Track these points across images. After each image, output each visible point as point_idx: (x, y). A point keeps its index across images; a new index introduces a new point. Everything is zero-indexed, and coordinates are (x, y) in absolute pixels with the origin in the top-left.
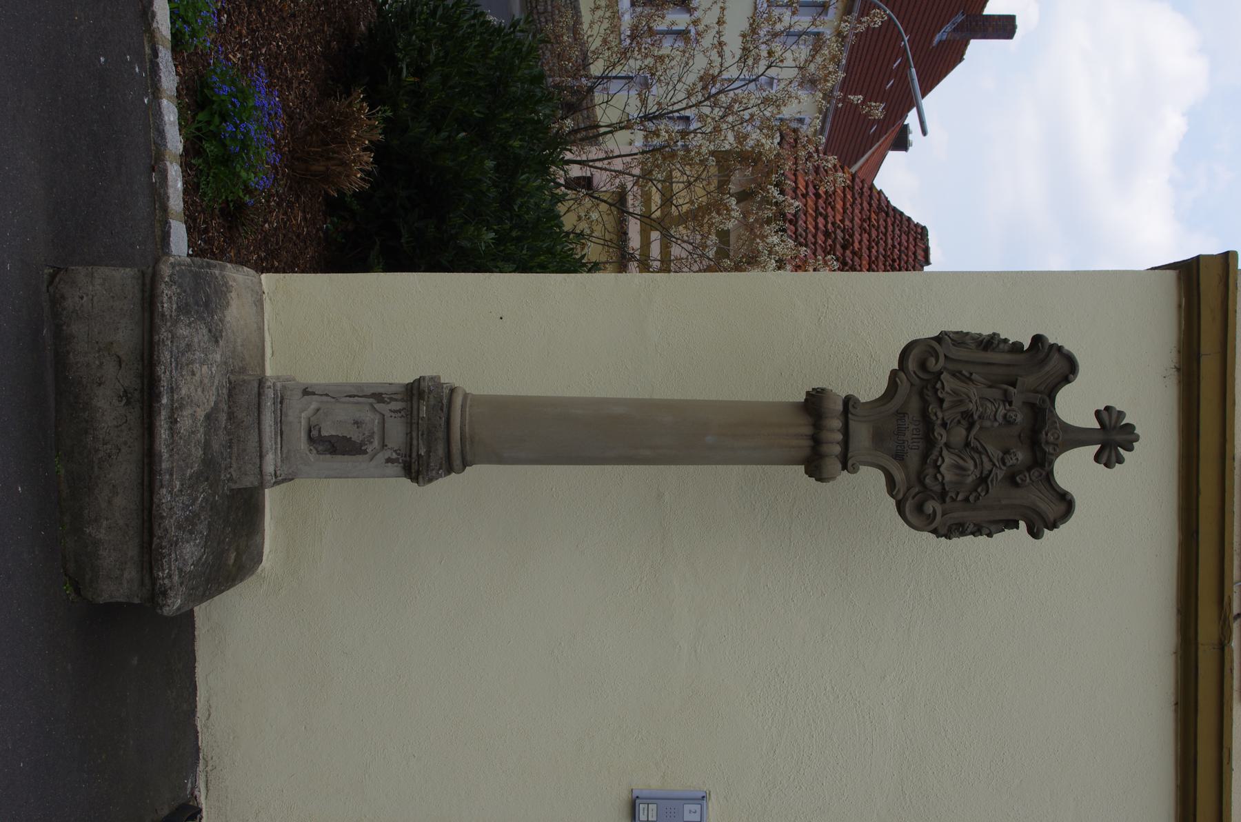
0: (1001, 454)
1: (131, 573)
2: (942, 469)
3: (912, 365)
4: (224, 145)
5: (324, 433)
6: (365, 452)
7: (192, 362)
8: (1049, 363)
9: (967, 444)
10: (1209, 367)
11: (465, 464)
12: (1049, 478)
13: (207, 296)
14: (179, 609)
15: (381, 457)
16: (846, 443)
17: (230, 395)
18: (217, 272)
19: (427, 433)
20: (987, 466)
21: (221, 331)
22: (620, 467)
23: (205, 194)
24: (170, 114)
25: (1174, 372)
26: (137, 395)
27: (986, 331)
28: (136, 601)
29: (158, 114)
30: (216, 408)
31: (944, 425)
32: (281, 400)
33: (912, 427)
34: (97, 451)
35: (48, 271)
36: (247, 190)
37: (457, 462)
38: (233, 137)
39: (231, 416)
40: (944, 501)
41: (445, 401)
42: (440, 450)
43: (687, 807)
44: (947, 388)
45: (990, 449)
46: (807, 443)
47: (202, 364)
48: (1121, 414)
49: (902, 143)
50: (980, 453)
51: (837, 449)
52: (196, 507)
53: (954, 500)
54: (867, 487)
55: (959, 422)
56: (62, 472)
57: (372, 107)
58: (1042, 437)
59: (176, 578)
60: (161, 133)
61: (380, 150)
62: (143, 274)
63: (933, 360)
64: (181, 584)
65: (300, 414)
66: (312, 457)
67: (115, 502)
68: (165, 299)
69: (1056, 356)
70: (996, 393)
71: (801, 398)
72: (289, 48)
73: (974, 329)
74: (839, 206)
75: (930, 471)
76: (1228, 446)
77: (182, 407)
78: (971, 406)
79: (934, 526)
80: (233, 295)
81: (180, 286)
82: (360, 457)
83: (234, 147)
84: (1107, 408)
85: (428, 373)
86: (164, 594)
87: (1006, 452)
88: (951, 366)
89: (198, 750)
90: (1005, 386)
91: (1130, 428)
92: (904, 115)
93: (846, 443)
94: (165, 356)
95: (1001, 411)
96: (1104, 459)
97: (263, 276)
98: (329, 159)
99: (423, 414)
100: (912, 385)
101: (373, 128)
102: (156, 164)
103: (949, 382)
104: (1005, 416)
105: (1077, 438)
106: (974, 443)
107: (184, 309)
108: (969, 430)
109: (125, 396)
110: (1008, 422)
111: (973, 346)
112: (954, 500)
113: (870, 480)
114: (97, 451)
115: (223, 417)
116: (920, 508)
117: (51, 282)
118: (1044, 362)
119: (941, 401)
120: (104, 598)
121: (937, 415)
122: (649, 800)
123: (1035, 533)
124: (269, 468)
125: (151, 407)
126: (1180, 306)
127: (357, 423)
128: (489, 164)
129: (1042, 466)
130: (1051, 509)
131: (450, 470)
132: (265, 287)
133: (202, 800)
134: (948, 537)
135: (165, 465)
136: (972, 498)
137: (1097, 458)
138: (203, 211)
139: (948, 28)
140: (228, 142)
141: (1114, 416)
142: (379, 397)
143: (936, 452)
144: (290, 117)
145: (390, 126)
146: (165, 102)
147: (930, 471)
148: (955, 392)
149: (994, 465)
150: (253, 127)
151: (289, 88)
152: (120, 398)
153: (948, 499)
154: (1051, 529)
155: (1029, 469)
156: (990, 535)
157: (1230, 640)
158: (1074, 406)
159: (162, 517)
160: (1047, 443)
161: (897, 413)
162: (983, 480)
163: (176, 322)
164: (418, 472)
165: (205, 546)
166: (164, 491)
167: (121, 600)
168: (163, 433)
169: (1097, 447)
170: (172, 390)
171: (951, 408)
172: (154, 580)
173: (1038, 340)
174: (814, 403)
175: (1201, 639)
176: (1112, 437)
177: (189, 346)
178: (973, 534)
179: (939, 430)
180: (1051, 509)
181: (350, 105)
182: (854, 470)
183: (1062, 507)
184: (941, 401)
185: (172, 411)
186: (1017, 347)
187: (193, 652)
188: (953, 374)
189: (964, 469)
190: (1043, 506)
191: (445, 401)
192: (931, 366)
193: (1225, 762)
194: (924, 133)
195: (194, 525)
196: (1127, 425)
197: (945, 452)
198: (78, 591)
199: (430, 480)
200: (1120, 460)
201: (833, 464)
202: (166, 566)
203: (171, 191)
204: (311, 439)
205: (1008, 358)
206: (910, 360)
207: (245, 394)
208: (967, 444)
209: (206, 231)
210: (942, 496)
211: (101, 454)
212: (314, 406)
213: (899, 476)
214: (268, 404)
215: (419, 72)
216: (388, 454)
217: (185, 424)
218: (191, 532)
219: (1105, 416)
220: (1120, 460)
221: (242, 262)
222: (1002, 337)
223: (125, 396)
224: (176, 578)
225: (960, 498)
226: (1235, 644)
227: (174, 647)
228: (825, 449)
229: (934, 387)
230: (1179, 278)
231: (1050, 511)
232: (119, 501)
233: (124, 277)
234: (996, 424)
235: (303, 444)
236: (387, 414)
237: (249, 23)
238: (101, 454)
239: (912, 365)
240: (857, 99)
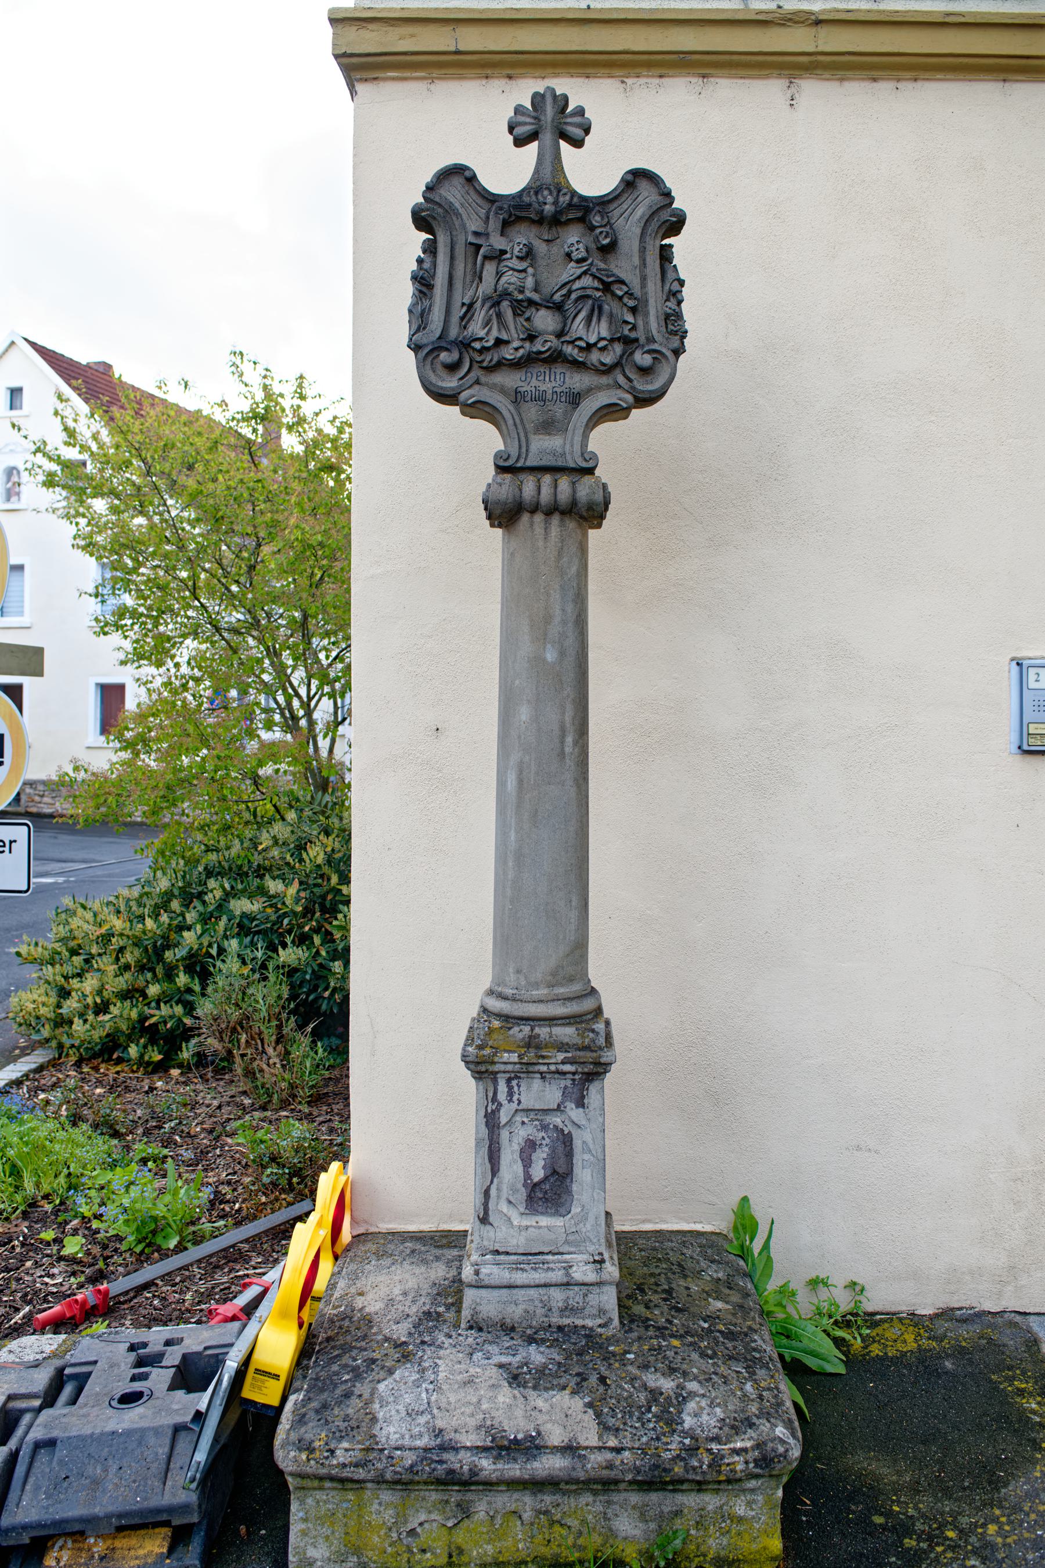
0: (572, 264)
2: (592, 341)
3: (450, 383)
10: (472, 40)
12: (604, 203)
19: (544, 1046)
33: (534, 383)
40: (636, 340)
44: (482, 333)
45: (565, 278)
48: (519, 110)
50: (570, 292)
51: (564, 484)
53: (634, 328)
54: (616, 448)
55: (528, 319)
58: (548, 209)
71: (499, 532)
75: (595, 357)
76: (570, 16)
84: (511, 129)
90: (480, 258)
100: (477, 382)
111: (427, 303)
113: (604, 440)
118: (450, 211)
119: (499, 342)
120: (776, 1545)
123: (676, 225)
136: (631, 303)
137: (578, 143)
142: (491, 1121)
143: (568, 350)
147: (595, 357)
149: (585, 273)
153: (633, 335)
156: (682, 283)
157: (811, 13)
158: (508, 171)
161: (515, 402)
169: (563, 145)
171: (507, 329)
173: (421, 220)
174: (503, 514)
176: (552, 126)
178: (679, 303)
179: (538, 346)
180: (646, 197)
182: (594, 456)
183: (644, 186)
184: (499, 342)
186: (430, 248)
192: (451, 360)
193: (963, 20)
200: (580, 111)
201: (585, 489)
206: (444, 385)
212: (504, 1207)
222: (414, 266)
225: (630, 318)
226: (816, 7)
234: (530, 270)
239: (450, 383)
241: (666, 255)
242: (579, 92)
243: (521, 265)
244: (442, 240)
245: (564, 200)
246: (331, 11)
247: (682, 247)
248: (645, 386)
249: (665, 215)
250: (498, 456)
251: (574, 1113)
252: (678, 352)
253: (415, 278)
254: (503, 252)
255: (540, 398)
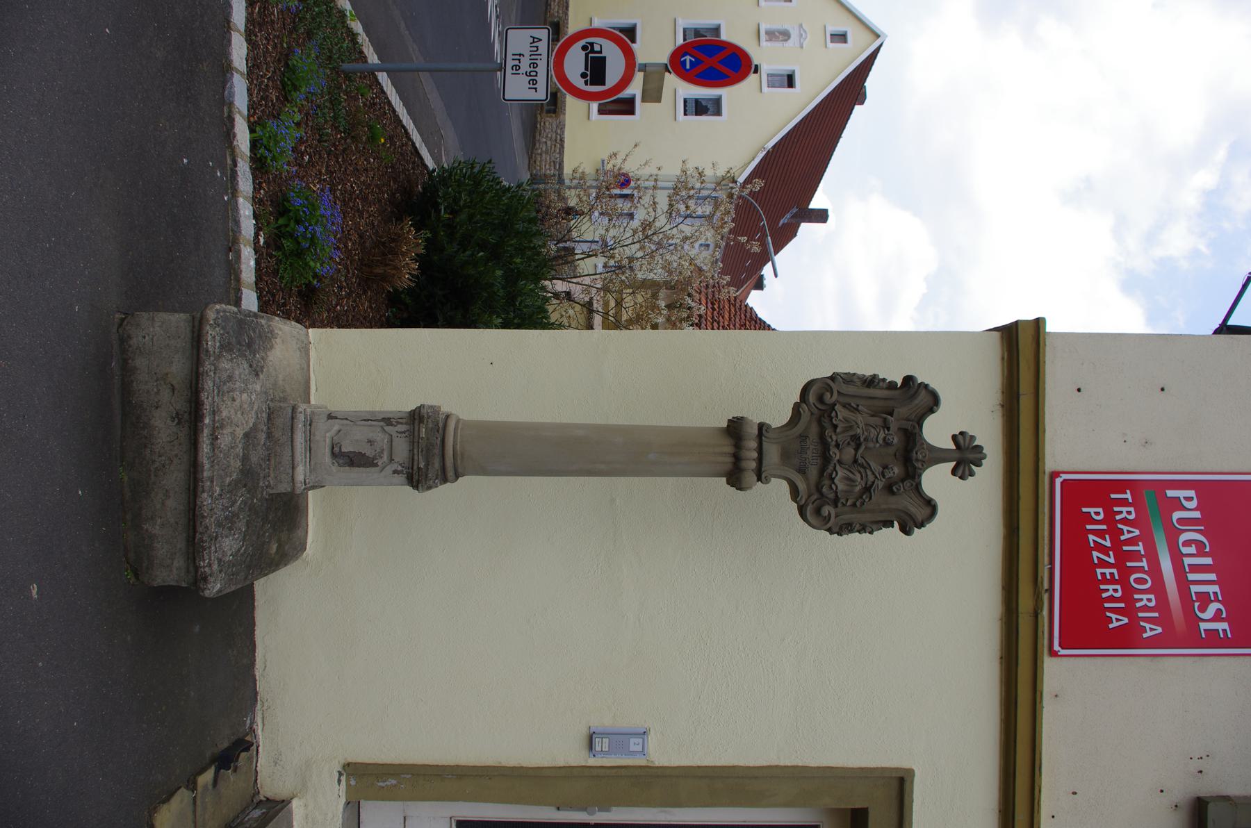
1: (179, 562)
3: (812, 398)
4: (299, 243)
5: (344, 450)
6: (376, 465)
7: (233, 390)
8: (916, 397)
9: (855, 461)
10: (1025, 403)
11: (457, 476)
12: (918, 488)
13: (251, 339)
14: (220, 591)
15: (389, 469)
16: (760, 460)
17: (269, 419)
18: (263, 322)
19: (427, 451)
20: (871, 478)
21: (262, 367)
22: (582, 478)
23: (282, 278)
24: (246, 210)
25: (999, 408)
26: (186, 416)
27: (868, 373)
28: (184, 585)
29: (236, 209)
30: (255, 428)
31: (837, 446)
32: (310, 423)
34: (154, 462)
35: (118, 316)
36: (315, 276)
37: (450, 474)
38: (304, 237)
39: (269, 435)
41: (441, 425)
42: (437, 465)
43: (632, 741)
45: (873, 465)
46: (730, 460)
47: (242, 392)
48: (973, 438)
49: (759, 285)
51: (754, 465)
52: (235, 509)
53: (844, 505)
54: (774, 496)
56: (126, 478)
57: (417, 230)
58: (912, 455)
59: (215, 567)
60: (237, 222)
61: (424, 261)
62: (193, 318)
63: (828, 395)
64: (221, 571)
65: (325, 434)
66: (335, 468)
67: (166, 506)
68: (209, 338)
69: (923, 392)
70: (877, 421)
71: (725, 425)
72: (361, 191)
73: (860, 372)
74: (727, 316)
75: (827, 482)
77: (222, 426)
78: (859, 431)
79: (829, 525)
80: (278, 340)
81: (223, 328)
82: (373, 469)
83: (305, 244)
84: (962, 433)
85: (429, 402)
86: (205, 579)
87: (885, 467)
88: (842, 400)
89: (256, 693)
91: (979, 449)
92: (761, 268)
93: (760, 460)
94: (209, 384)
95: (882, 435)
96: (960, 473)
97: (310, 330)
98: (386, 265)
99: (423, 434)
101: (418, 245)
102: (232, 245)
103: (841, 412)
104: (884, 439)
105: (938, 456)
106: (860, 460)
107: (226, 347)
108: (857, 449)
109: (177, 417)
110: (887, 443)
112: (844, 505)
113: (778, 489)
114: (154, 462)
115: (262, 437)
116: (818, 511)
117: (120, 325)
119: (835, 427)
120: (158, 582)
121: (832, 438)
122: (604, 734)
123: (906, 530)
124: (300, 477)
125: (196, 425)
126: (1003, 358)
127: (370, 442)
128: (499, 273)
129: (913, 478)
130: (919, 512)
131: (445, 480)
132: (311, 339)
133: (259, 732)
134: (840, 534)
135: (205, 474)
137: (954, 472)
138: (281, 289)
139: (788, 216)
140: (300, 239)
141: (968, 439)
142: (388, 421)
143: (831, 468)
144: (361, 236)
145: (431, 244)
146: (241, 200)
148: (846, 420)
150: (319, 229)
151: (361, 216)
152: (173, 419)
154: (919, 528)
155: (903, 481)
156: (871, 533)
159: (203, 517)
160: (917, 460)
162: (867, 489)
163: (219, 357)
164: (418, 482)
165: (244, 540)
166: (205, 495)
167: (172, 583)
168: (205, 448)
169: (953, 464)
170: (214, 413)
171: (843, 432)
172: (197, 568)
173: (908, 380)
174: (735, 428)
175: (1021, 609)
176: (965, 456)
177: (230, 378)
178: (859, 532)
179: (833, 450)
180: (919, 512)
181: (402, 229)
182: (767, 481)
183: (928, 511)
184: (835, 427)
185: (214, 429)
186: (892, 385)
187: (253, 618)
188: (844, 406)
189: (853, 481)
190: (913, 510)
191: (441, 425)
194: (776, 276)
195: (233, 523)
196: (977, 446)
197: (838, 467)
198: (136, 576)
199: (429, 488)
200: (972, 474)
201: (750, 477)
202: (206, 557)
203: (243, 267)
204: (333, 454)
205: (886, 393)
207: (281, 418)
208: (855, 461)
209: (284, 305)
210: (835, 503)
211: (157, 464)
212: (336, 428)
213: (802, 486)
214: (300, 426)
215: (454, 213)
216: (395, 466)
217: (225, 440)
218: (230, 529)
219: (960, 438)
220: (972, 474)
221: (287, 316)
223: (177, 417)
224: (215, 567)
227: (238, 611)
228: (744, 464)
229: (830, 416)
230: (1002, 337)
231: (916, 514)
232: (170, 503)
233: (178, 320)
235: (328, 458)
236: (394, 435)
237: (328, 166)
238: (157, 464)
239: (812, 398)
240: (744, 239)
241: (889, 524)
242: (990, 473)
243: (881, 441)
244: (897, 392)
245: (918, 465)
246: (1043, 319)
247: (893, 533)
248: (809, 509)
249: (910, 523)
250: (769, 426)
251: (389, 469)
252: (830, 531)
253: (875, 376)
254: (888, 429)
255: (803, 451)
